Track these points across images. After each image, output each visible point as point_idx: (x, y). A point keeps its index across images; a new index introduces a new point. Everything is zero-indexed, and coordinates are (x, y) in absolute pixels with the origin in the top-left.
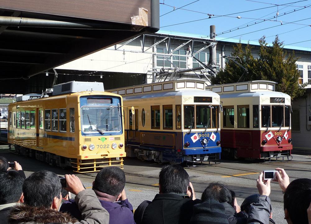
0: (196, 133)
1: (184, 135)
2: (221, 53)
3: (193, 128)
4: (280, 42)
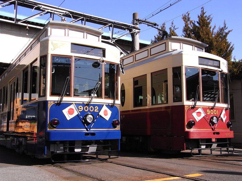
1: (49, 106)
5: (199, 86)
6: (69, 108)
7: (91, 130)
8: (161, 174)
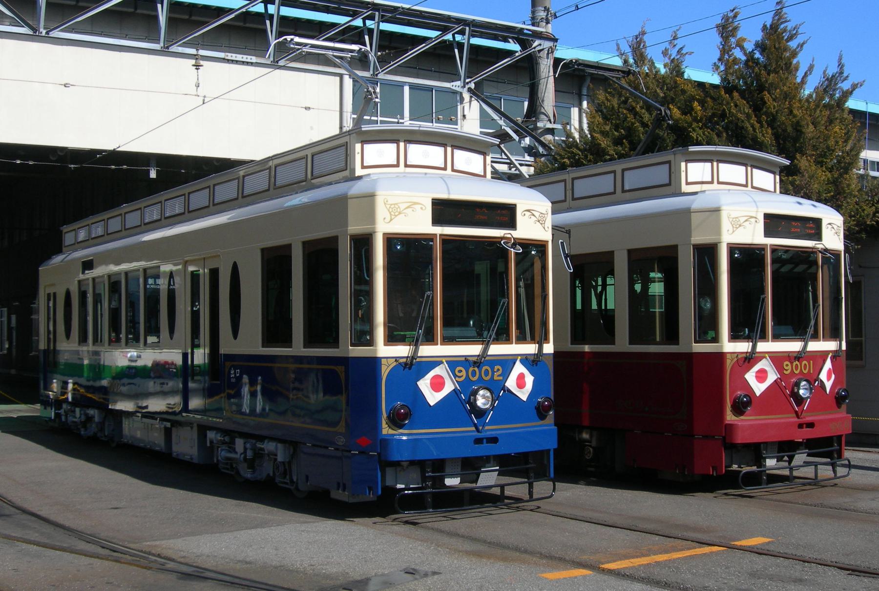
0: (441, 363)
1: (385, 371)
2: (576, 102)
3: (430, 339)
4: (789, 28)
5: (763, 299)
6: (432, 374)
7: (487, 428)
8: (685, 542)
